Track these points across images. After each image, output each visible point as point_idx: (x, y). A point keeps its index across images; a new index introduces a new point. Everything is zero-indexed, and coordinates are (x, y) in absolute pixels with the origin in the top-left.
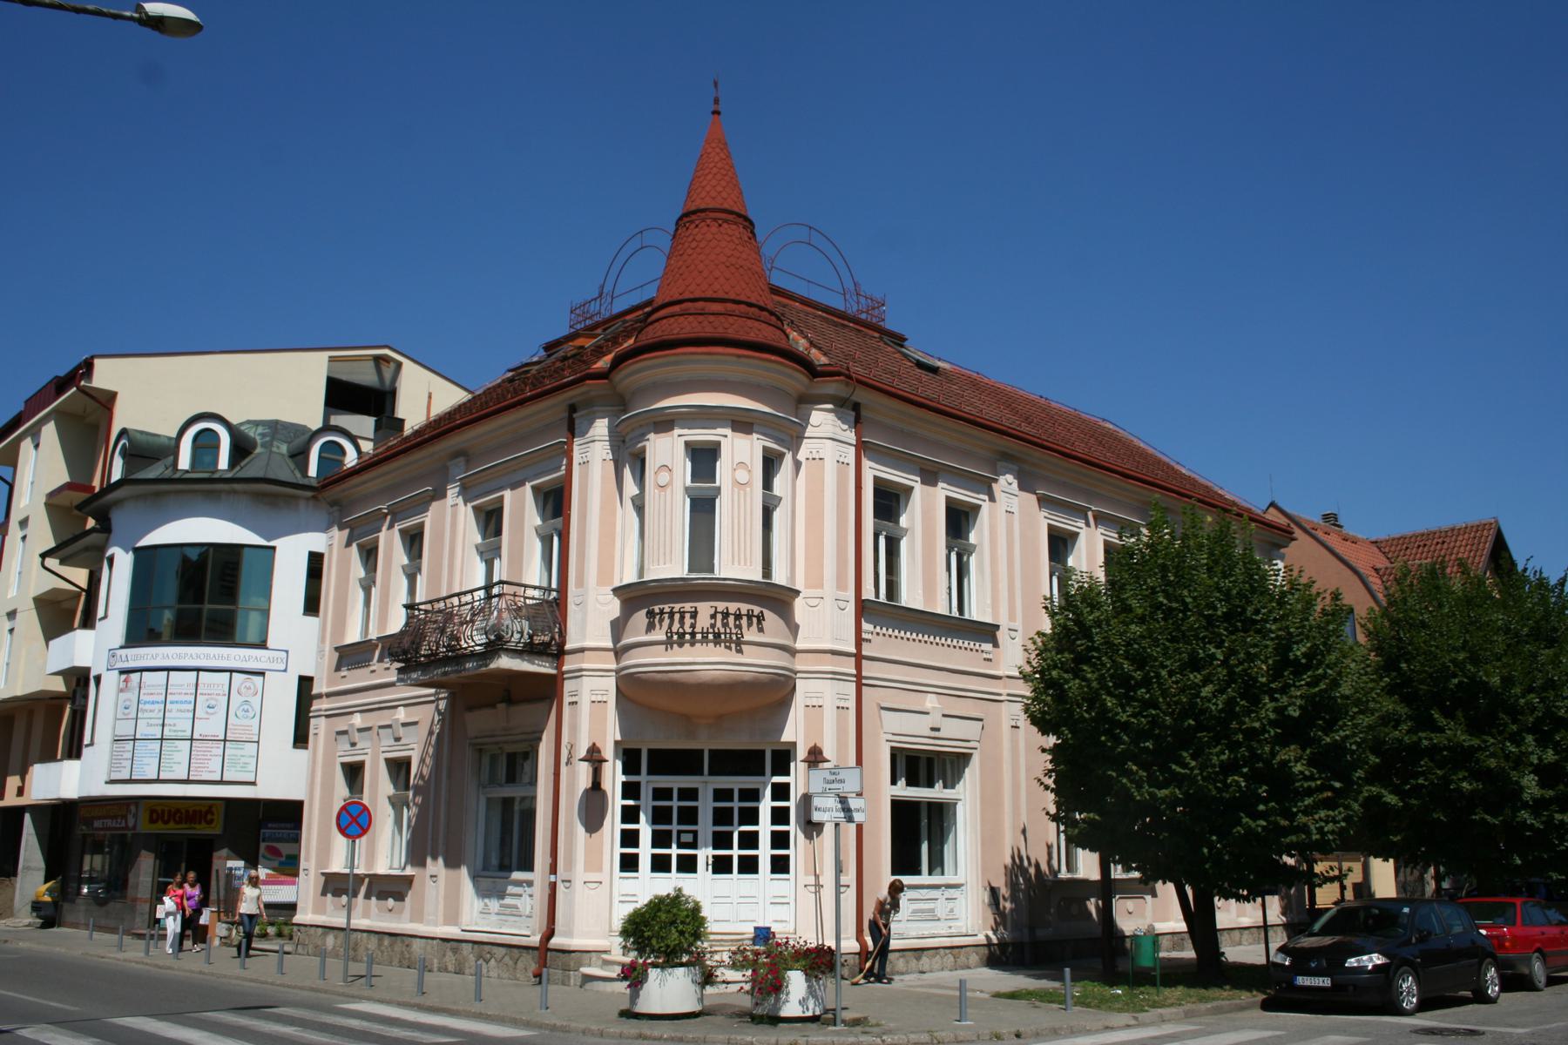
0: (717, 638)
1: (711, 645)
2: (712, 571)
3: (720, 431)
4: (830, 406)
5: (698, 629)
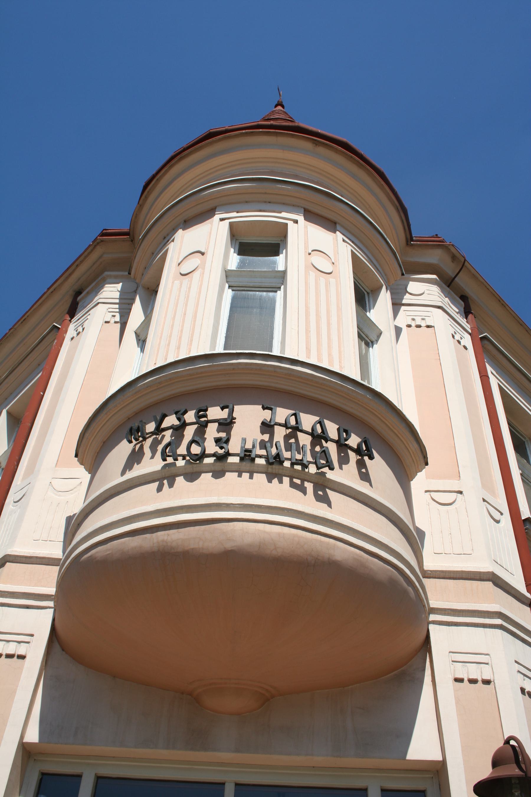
0: (274, 467)
1: (261, 478)
2: (270, 349)
3: (284, 214)
4: (434, 276)
5: (235, 446)
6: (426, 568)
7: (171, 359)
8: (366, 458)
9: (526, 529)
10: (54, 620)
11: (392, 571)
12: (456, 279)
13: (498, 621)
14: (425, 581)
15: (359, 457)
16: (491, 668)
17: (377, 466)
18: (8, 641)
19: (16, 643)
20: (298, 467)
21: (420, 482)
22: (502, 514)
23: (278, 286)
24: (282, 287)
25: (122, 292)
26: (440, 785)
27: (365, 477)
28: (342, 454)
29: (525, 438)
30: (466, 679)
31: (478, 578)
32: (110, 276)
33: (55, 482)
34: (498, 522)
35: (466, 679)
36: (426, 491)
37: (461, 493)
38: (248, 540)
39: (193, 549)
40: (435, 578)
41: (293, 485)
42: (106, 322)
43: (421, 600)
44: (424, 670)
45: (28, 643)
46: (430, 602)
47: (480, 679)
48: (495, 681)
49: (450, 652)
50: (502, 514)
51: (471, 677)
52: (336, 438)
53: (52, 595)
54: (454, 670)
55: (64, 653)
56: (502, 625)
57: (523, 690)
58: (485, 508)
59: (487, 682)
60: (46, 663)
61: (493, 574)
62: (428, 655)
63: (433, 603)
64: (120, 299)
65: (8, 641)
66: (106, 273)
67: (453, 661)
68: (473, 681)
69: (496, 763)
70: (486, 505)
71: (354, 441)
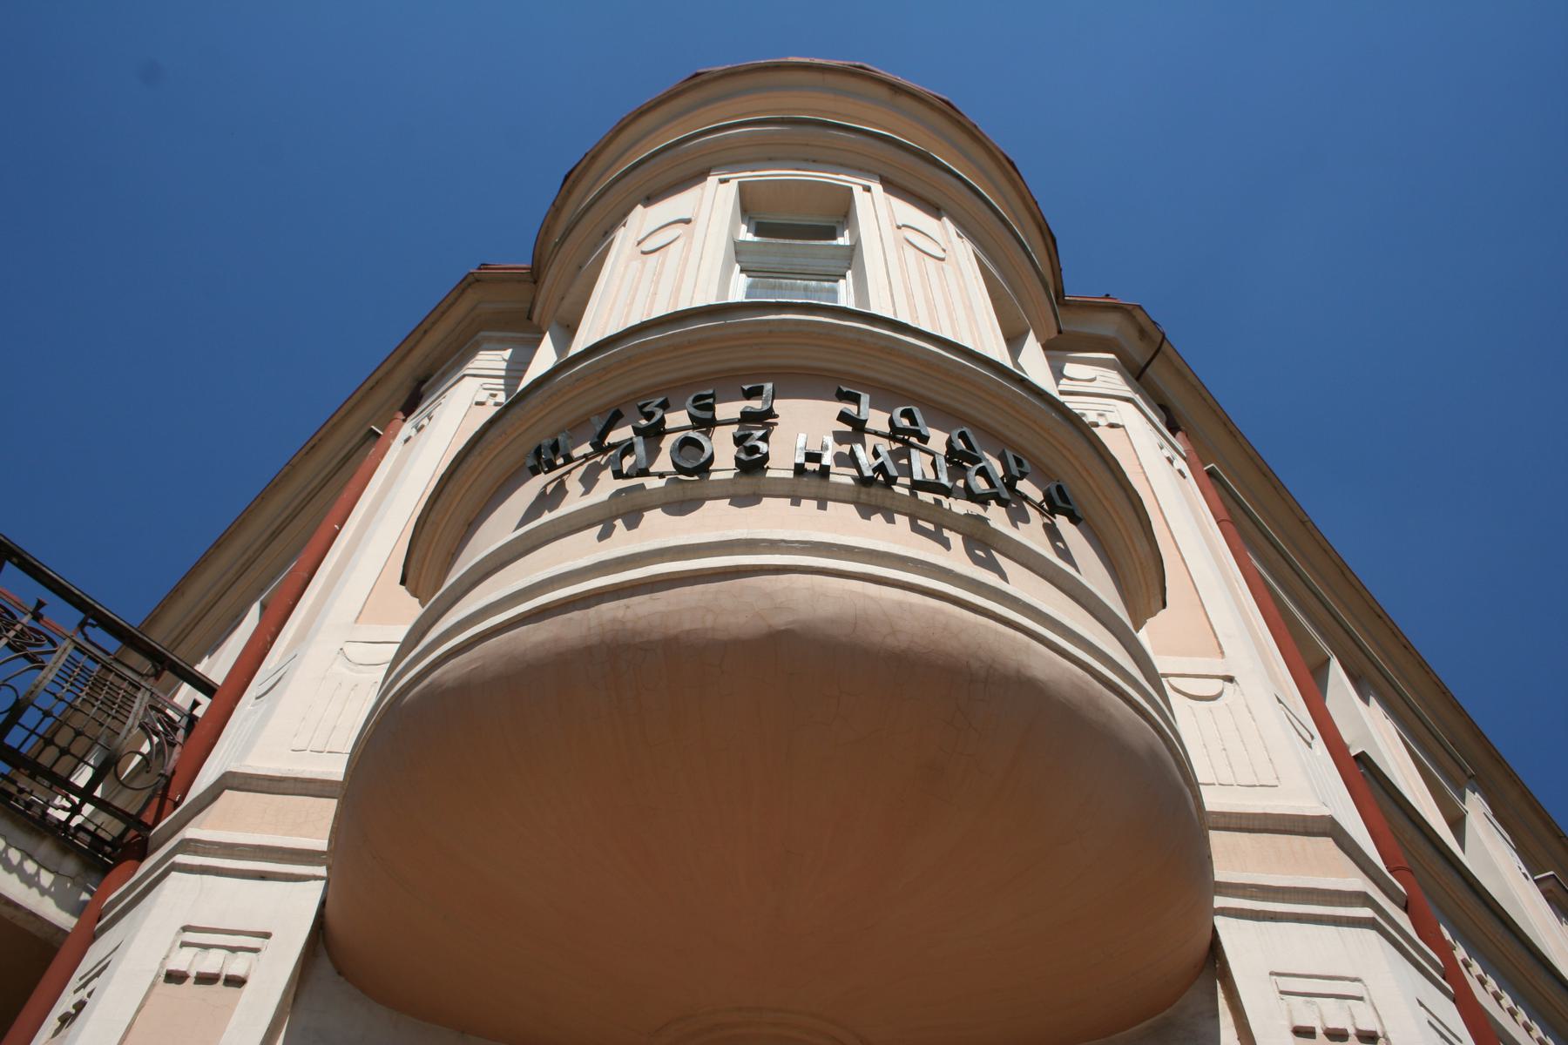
7: (634, 321)
10: (323, 904)
12: (1149, 370)
13: (1367, 912)
16: (1371, 1009)
18: (206, 947)
19: (225, 952)
20: (926, 497)
23: (840, 271)
24: (849, 274)
25: (510, 362)
32: (489, 340)
33: (351, 650)
35: (1319, 1031)
37: (1230, 679)
38: (826, 610)
39: (688, 632)
41: (916, 528)
42: (478, 404)
44: (1215, 1015)
45: (256, 950)
47: (1351, 1031)
48: (1390, 1035)
49: (1272, 974)
51: (1331, 1025)
53: (323, 853)
55: (342, 979)
60: (295, 999)
63: (1221, 875)
64: (507, 370)
65: (206, 947)
66: (482, 333)
67: (1282, 992)
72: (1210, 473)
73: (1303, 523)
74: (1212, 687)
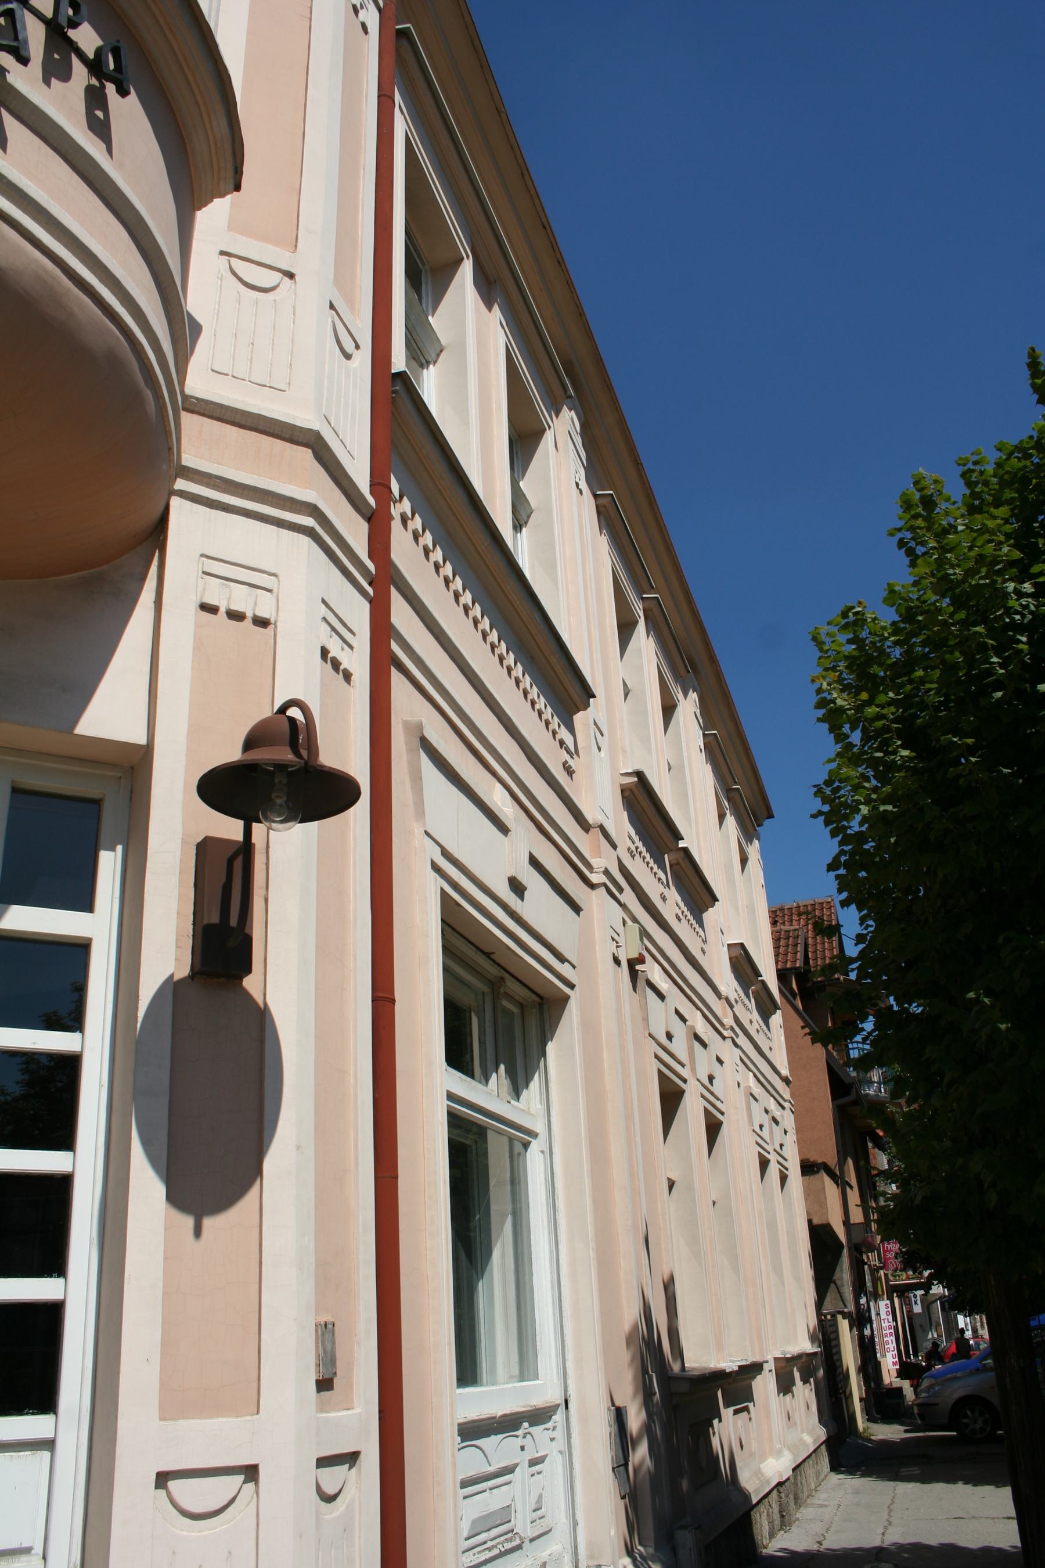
6: (188, 391)
8: (110, 89)
9: (393, 392)
11: (118, 338)
13: (309, 521)
14: (186, 418)
15: (94, 82)
16: (274, 601)
17: (127, 112)
21: (214, 218)
22: (357, 347)
26: (132, 792)
27: (101, 129)
28: (56, 56)
29: (424, 264)
30: (223, 610)
31: (287, 436)
34: (348, 357)
35: (223, 610)
36: (222, 253)
37: (291, 276)
40: (203, 415)
43: (167, 433)
46: (184, 456)
47: (249, 614)
48: (278, 624)
49: (202, 555)
50: (357, 347)
51: (233, 608)
52: (49, 13)
54: (204, 590)
56: (313, 529)
57: (324, 652)
58: (330, 320)
59: (262, 623)
61: (317, 435)
62: (157, 554)
63: (188, 459)
67: (204, 573)
68: (236, 616)
69: (249, 744)
70: (332, 317)
71: (87, 38)
72: (403, 34)
73: (499, 112)
74: (268, 278)
